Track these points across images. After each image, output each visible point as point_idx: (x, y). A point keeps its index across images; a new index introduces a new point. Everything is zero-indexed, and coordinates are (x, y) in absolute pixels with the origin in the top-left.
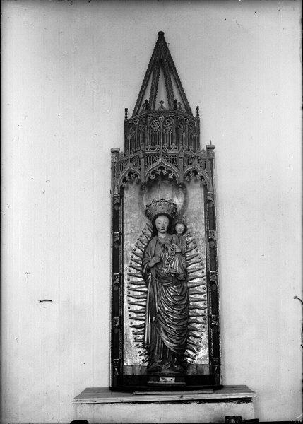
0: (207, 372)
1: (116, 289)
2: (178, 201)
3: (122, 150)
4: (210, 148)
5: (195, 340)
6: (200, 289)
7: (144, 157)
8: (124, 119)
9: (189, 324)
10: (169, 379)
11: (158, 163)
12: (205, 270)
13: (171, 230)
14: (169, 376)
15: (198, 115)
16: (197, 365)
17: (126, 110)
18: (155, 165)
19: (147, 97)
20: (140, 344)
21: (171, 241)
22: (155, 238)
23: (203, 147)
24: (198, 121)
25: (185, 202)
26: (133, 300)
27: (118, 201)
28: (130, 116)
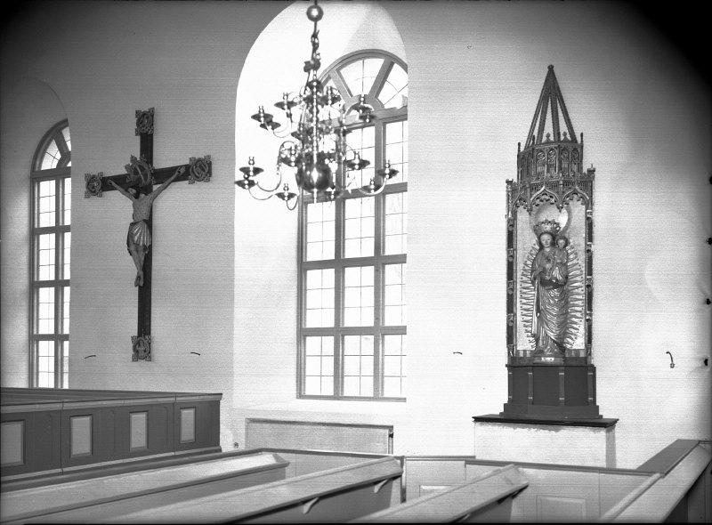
0: (582, 355)
1: (511, 260)
2: (562, 220)
3: (515, 180)
4: (592, 171)
5: (573, 331)
6: (579, 290)
7: (530, 187)
8: (313, 31)
9: (568, 328)
10: (549, 359)
11: (542, 189)
12: (584, 276)
13: (554, 244)
14: (549, 356)
15: (582, 141)
16: (575, 350)
17: (519, 144)
18: (538, 193)
19: (536, 133)
20: (530, 334)
21: (554, 255)
22: (541, 253)
23: (585, 170)
24: (582, 147)
25: (569, 220)
26: (524, 301)
27: (511, 223)
28: (522, 149)
